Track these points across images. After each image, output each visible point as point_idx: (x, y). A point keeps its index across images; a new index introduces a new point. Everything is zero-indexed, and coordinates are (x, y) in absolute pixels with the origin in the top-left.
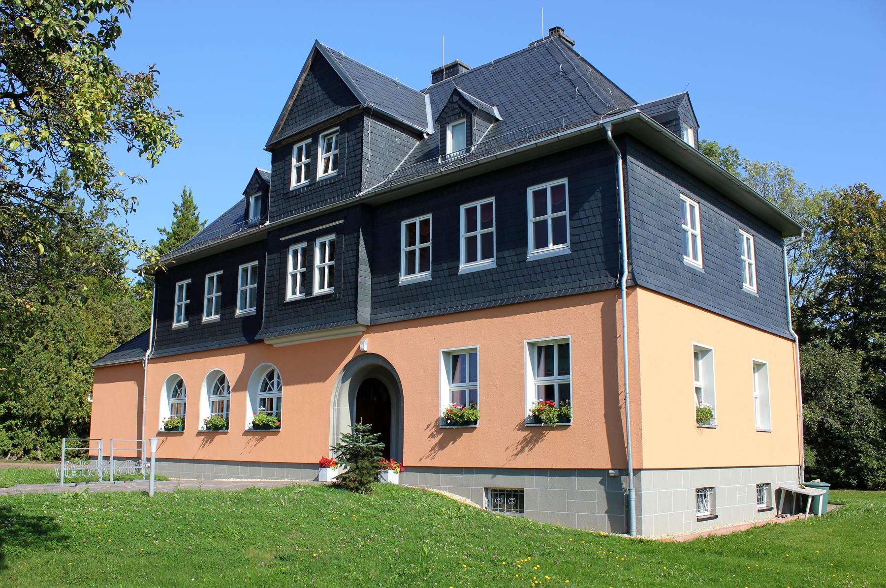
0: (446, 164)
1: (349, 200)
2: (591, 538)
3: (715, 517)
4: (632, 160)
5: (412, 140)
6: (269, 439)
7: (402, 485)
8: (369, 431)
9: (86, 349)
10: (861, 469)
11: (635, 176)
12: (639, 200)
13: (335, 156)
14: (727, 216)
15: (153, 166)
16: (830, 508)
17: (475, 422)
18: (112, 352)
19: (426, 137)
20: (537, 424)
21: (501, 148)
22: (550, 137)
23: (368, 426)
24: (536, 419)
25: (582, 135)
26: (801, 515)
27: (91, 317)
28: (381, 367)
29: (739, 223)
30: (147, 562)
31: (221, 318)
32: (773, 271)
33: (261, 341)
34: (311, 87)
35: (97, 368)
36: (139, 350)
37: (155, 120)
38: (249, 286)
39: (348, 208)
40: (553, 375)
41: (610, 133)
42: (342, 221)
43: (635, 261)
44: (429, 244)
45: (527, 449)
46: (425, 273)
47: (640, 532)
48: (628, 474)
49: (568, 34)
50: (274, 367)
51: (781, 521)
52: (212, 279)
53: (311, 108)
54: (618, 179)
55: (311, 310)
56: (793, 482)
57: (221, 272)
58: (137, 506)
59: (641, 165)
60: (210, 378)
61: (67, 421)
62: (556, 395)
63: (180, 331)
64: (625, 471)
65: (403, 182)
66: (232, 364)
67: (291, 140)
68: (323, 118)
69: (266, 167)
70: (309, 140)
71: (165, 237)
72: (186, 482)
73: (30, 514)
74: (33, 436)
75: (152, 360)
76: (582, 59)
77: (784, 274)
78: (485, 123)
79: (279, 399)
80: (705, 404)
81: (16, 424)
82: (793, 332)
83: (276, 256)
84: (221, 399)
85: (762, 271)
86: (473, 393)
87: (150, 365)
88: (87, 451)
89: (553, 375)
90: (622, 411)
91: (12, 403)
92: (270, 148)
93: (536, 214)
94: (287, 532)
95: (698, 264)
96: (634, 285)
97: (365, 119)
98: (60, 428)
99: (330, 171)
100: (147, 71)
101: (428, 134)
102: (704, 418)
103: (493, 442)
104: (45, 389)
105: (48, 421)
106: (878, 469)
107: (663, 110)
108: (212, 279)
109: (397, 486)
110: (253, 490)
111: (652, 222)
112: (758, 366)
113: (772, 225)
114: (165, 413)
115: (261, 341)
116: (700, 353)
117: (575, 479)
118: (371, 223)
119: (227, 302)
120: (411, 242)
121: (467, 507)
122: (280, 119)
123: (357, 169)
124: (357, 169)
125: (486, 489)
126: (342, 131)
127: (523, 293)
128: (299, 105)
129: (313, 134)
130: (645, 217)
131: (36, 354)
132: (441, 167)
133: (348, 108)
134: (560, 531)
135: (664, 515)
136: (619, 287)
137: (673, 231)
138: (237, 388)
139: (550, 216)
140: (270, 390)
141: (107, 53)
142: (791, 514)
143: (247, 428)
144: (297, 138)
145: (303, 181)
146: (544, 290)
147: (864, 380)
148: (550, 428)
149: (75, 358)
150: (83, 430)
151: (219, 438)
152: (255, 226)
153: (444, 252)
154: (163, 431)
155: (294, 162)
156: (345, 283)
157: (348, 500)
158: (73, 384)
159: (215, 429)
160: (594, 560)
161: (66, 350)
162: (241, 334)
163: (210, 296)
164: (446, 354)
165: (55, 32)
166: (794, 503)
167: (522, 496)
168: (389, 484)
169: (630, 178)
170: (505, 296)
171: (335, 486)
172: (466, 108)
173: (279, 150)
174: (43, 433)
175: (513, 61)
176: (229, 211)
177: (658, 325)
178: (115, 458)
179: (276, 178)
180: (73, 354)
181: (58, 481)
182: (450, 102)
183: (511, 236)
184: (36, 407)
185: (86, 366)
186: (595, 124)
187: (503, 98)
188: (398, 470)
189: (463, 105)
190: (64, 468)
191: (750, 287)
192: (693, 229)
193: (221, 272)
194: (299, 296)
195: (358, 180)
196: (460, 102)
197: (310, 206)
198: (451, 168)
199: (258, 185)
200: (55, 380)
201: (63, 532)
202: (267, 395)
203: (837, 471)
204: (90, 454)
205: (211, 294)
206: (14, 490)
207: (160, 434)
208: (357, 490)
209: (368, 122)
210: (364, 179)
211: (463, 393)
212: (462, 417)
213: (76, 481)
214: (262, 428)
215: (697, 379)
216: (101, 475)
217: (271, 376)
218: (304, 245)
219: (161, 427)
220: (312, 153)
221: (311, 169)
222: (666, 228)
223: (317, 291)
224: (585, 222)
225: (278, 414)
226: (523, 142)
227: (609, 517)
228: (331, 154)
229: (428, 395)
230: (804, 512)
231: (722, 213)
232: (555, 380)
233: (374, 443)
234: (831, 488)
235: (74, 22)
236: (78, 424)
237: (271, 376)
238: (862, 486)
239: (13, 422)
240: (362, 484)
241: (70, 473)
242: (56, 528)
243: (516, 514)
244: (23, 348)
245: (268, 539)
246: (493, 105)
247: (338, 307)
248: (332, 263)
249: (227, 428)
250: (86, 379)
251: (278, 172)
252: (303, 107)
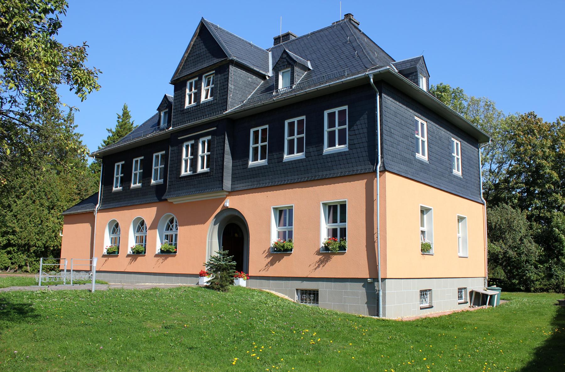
0: (277, 95)
1: (220, 116)
2: (354, 318)
3: (431, 307)
4: (386, 96)
5: (259, 80)
6: (170, 259)
7: (248, 287)
8: (227, 254)
9: (59, 203)
10: (526, 280)
11: (387, 106)
12: (389, 120)
13: (212, 89)
14: (444, 130)
15: (82, 101)
16: (501, 302)
17: (291, 250)
18: (76, 205)
19: (267, 78)
20: (327, 252)
21: (309, 87)
22: (337, 81)
23: (227, 252)
24: (326, 248)
25: (356, 81)
26: (484, 307)
27: (63, 184)
28: (237, 216)
29: (452, 134)
30: (84, 329)
31: (142, 185)
32: (472, 162)
33: (166, 200)
34: (199, 46)
35: (66, 215)
36: (92, 204)
37: (84, 75)
38: (159, 167)
39: (219, 121)
40: (337, 222)
41: (372, 80)
42: (215, 128)
43: (385, 156)
44: (266, 143)
45: (321, 266)
46: (301, 154)
47: (384, 315)
48: (378, 281)
49: (355, 18)
50: (174, 216)
51: (472, 309)
52: (137, 162)
53: (198, 59)
54: (376, 107)
55: (196, 181)
56: (480, 287)
57: (142, 158)
58: (83, 298)
59: (391, 99)
60: (135, 222)
61: (46, 248)
62: (338, 234)
63: (117, 193)
64: (376, 279)
65: (251, 106)
66: (148, 214)
67: (186, 78)
68: (205, 65)
69: (171, 94)
70: (197, 79)
71: (111, 135)
72: (115, 285)
73: (15, 303)
74: (25, 257)
75: (100, 211)
76: (363, 33)
77: (479, 165)
78: (302, 71)
79: (176, 235)
80: (427, 241)
81: (14, 250)
82: (483, 199)
83: (175, 148)
84: (142, 235)
85: (465, 163)
86: (290, 233)
88: (59, 267)
89: (337, 222)
90: (376, 244)
91: (10, 236)
92: (173, 82)
93: (330, 127)
94: (171, 313)
95: (425, 158)
96: (384, 170)
97: (230, 66)
98: (42, 252)
99: (209, 97)
100: (81, 45)
101: (269, 77)
102: (426, 249)
103: (301, 262)
104: (33, 228)
105: (35, 248)
106: (537, 280)
107: (408, 66)
108: (137, 162)
109: (244, 288)
110: (155, 289)
112: (460, 219)
113: (472, 136)
114: (107, 243)
115: (166, 200)
116: (424, 211)
117: (348, 284)
118: (232, 130)
119: (146, 175)
120: (291, 133)
121: (283, 299)
122: (180, 65)
123: (225, 97)
124: (225, 97)
125: (297, 290)
126: (216, 74)
127: (320, 173)
128: (191, 57)
130: (392, 130)
131: (27, 205)
132: (275, 97)
133: (220, 60)
134: (336, 314)
135: (400, 305)
136: (375, 171)
137: (410, 139)
138: (151, 228)
139: (296, 137)
140: (171, 230)
141: (54, 37)
142: (479, 305)
143: (157, 253)
144: (189, 77)
145: (192, 103)
146: (332, 172)
147: (531, 227)
148: (335, 254)
149: (52, 209)
150: (57, 253)
151: (140, 259)
152: (163, 129)
153: (275, 147)
154: (106, 253)
155: (188, 91)
156: (216, 166)
157: (214, 295)
158: (51, 225)
159: (138, 253)
160: (352, 330)
161: (47, 204)
162: (155, 195)
163: (136, 172)
164: (275, 209)
165: (21, 24)
166: (479, 299)
167: (318, 294)
168: (239, 286)
169: (383, 107)
170: (310, 175)
171: (207, 287)
172: (291, 62)
173: (179, 83)
174: (31, 255)
175: (322, 33)
176: (149, 120)
177: (398, 194)
178: (73, 270)
179: (176, 101)
180: (51, 207)
181: (37, 284)
182: (281, 58)
183: (314, 139)
184: (27, 239)
185: (59, 214)
186: (364, 74)
187: (314, 56)
188: (246, 278)
189: (289, 60)
190: (41, 277)
191: (457, 172)
192: (423, 137)
193: (142, 158)
194: (189, 173)
195: (225, 104)
196: (287, 58)
197: (196, 119)
198: (280, 98)
199: (166, 105)
200: (39, 222)
201: (36, 313)
202: (169, 233)
203: (514, 281)
204: (61, 268)
205: (136, 171)
206: (7, 290)
207: (104, 256)
208: (219, 289)
209: (232, 69)
210: (229, 103)
211: (285, 232)
212: (283, 247)
213: (49, 284)
214: (166, 253)
215: (422, 225)
216: (65, 280)
217: (172, 221)
218: (193, 142)
219: (105, 252)
220: (198, 86)
221: (198, 96)
222: (406, 137)
223: (199, 170)
224: (357, 132)
225: (176, 244)
226: (323, 84)
227: (368, 306)
228: (209, 87)
229: (264, 232)
230: (486, 304)
231: (441, 128)
232: (338, 225)
233: (229, 262)
234: (502, 291)
235: (33, 19)
236: (54, 250)
237: (172, 221)
238: (528, 290)
239: (11, 249)
240: (222, 286)
241: (45, 279)
242: (32, 310)
243: (313, 305)
244: (18, 203)
245: (159, 317)
246: (308, 60)
247: (211, 180)
248: (209, 153)
249: (145, 253)
250: (59, 222)
251: (178, 97)
252: (193, 58)
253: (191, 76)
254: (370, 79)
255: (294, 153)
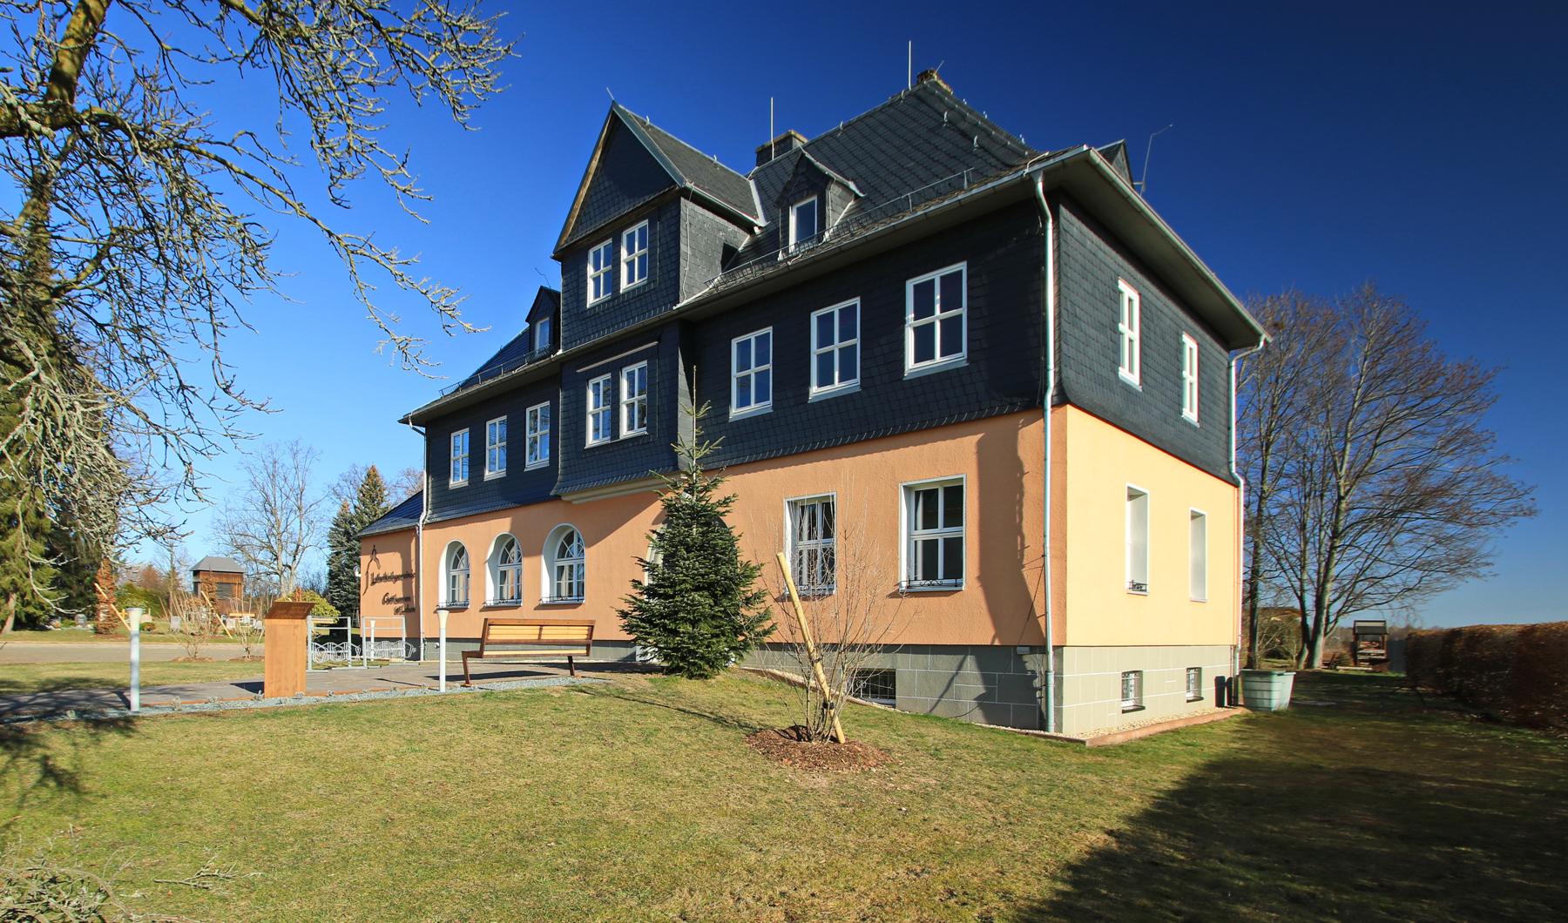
1: (663, 313)
12: (1071, 285)
19: (756, 230)
33: (557, 498)
41: (1040, 186)
47: (1059, 727)
69: (557, 284)
75: (430, 525)
87: (430, 532)
96: (1063, 399)
111: (1085, 318)
129: (613, 232)
139: (837, 346)
155: (590, 270)
164: (793, 504)
173: (570, 257)
202: (565, 563)
209: (687, 207)
218: (608, 376)
223: (625, 432)
237: (569, 539)
247: (653, 453)
253: (597, 237)
254: (1034, 186)
255: (749, 404)
